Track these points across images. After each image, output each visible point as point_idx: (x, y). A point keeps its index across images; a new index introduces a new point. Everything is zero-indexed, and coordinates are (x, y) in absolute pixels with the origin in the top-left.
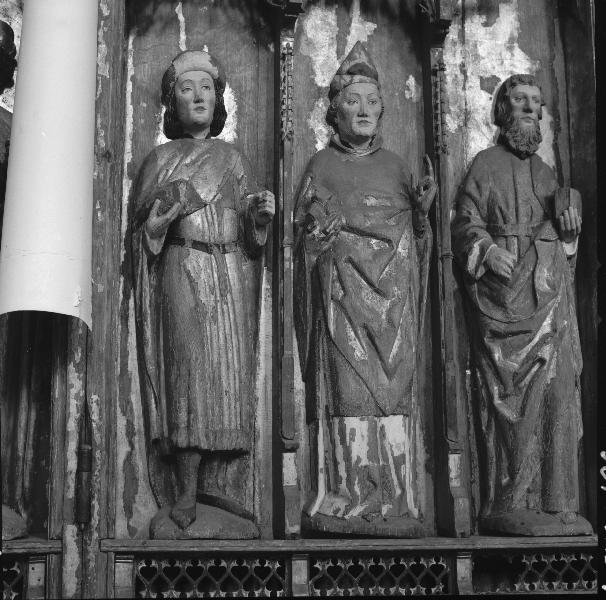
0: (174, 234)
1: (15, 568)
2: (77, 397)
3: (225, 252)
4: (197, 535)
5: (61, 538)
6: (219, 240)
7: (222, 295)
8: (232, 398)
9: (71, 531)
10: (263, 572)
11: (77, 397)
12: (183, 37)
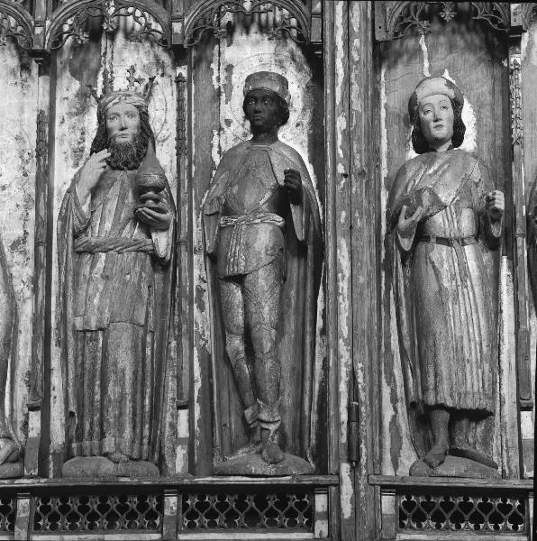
0: (422, 233)
1: (305, 499)
3: (464, 244)
5: (338, 474)
6: (457, 235)
7: (462, 281)
8: (474, 365)
10: (505, 508)
11: (346, 366)
12: (426, 64)
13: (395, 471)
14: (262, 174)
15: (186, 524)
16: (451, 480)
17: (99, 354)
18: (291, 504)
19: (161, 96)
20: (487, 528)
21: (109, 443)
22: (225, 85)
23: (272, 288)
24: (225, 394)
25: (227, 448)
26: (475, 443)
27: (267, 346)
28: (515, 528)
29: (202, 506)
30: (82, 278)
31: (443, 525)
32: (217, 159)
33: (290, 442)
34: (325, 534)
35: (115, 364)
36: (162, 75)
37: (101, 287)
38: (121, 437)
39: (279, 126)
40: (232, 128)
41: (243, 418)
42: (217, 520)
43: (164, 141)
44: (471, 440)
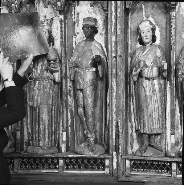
0: (140, 75)
1: (102, 161)
2: (115, 120)
3: (154, 80)
4: (146, 156)
5: (112, 155)
6: (152, 77)
7: (153, 92)
8: (156, 120)
9: (114, 153)
10: (164, 166)
11: (115, 120)
12: (144, 13)
13: (132, 150)
14: (88, 54)
15: (66, 168)
16: (147, 158)
17: (37, 115)
18: (98, 162)
19: (56, 24)
20: (158, 171)
21: (41, 144)
22: (77, 20)
23: (92, 94)
24: (78, 125)
25: (79, 142)
26: (157, 142)
27: (90, 113)
28: (167, 172)
29: (71, 162)
30: (31, 89)
31: (145, 170)
32: (74, 46)
33: (99, 141)
34: (108, 172)
35: (42, 119)
36: (56, 16)
37: (37, 93)
38: (45, 141)
39: (94, 35)
40: (79, 35)
41: (84, 133)
42: (76, 167)
43: (57, 39)
44: (156, 141)
